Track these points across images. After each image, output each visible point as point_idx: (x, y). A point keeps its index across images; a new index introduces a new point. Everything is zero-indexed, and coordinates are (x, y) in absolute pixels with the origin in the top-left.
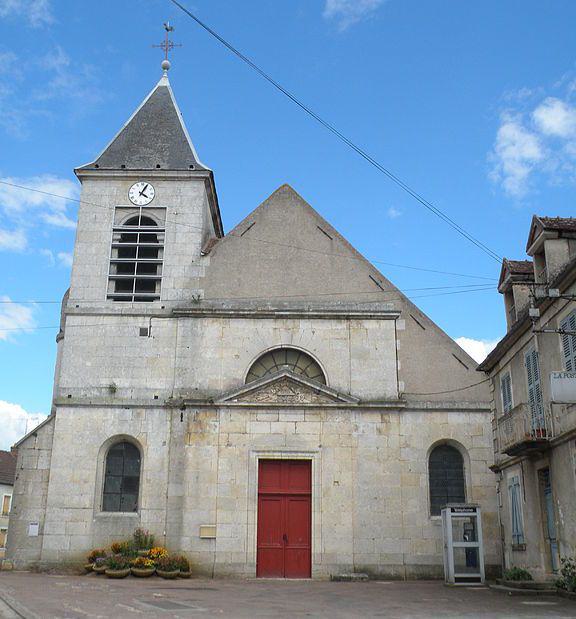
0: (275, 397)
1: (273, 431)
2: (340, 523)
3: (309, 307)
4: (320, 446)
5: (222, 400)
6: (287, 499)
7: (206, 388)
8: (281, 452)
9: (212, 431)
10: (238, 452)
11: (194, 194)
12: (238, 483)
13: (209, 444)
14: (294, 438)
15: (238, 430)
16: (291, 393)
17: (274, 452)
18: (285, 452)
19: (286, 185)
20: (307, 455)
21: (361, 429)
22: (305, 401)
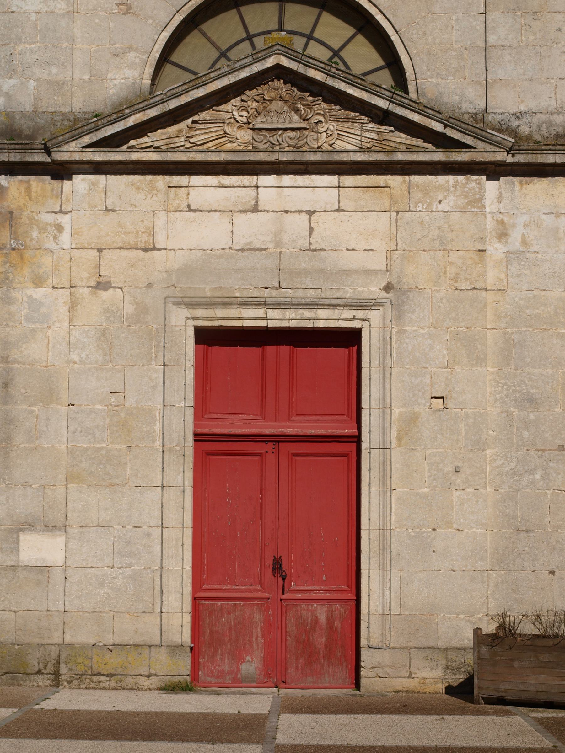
0: (245, 136)
1: (240, 242)
2: (449, 524)
3: (508, 696)
4: (388, 288)
5: (73, 146)
6: (286, 448)
7: (28, 108)
8: (265, 305)
9: (50, 244)
10: (129, 309)
11: (530, 40)
12: (130, 402)
13: (38, 282)
14: (304, 262)
15: (132, 240)
16: (296, 121)
17: (244, 304)
18: (278, 305)
19: (480, 629)
20: (347, 314)
21: (515, 236)
22: (339, 145)
